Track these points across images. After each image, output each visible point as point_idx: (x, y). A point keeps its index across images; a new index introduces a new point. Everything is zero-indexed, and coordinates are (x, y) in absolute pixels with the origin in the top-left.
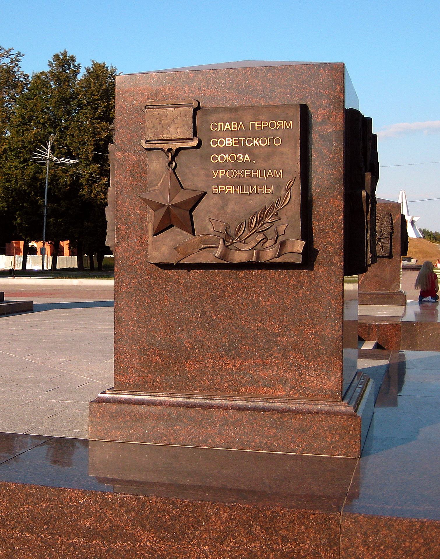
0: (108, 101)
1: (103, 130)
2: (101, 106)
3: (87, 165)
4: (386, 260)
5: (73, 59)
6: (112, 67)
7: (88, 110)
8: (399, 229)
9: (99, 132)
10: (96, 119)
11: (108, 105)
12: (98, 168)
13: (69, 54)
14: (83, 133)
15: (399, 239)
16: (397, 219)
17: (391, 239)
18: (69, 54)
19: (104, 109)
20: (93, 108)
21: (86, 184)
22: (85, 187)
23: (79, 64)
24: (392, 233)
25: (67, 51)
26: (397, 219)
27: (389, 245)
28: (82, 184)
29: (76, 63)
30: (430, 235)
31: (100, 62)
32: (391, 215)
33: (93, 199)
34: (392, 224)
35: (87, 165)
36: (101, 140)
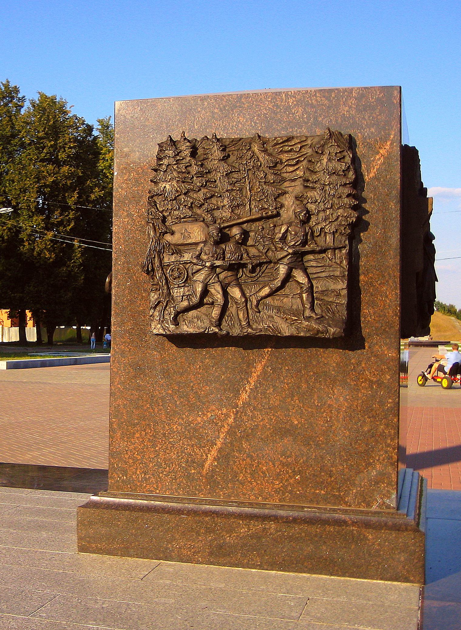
0: (56, 140)
1: (49, 175)
2: (47, 146)
3: (30, 217)
4: (333, 358)
5: (16, 90)
6: (62, 99)
7: (31, 150)
8: (394, 207)
9: (44, 177)
10: (42, 160)
11: (55, 145)
12: (43, 220)
13: (12, 85)
14: (25, 178)
15: (393, 260)
16: (379, 166)
17: (353, 259)
18: (12, 85)
19: (51, 149)
20: (37, 149)
21: (27, 240)
22: (26, 244)
23: (24, 97)
24: (357, 228)
25: (9, 80)
26: (379, 166)
27: (342, 286)
28: (22, 241)
29: (20, 95)
30: (444, 307)
31: (49, 95)
32: (351, 143)
33: (36, 259)
34: (358, 183)
35: (30, 217)
36: (45, 186)
